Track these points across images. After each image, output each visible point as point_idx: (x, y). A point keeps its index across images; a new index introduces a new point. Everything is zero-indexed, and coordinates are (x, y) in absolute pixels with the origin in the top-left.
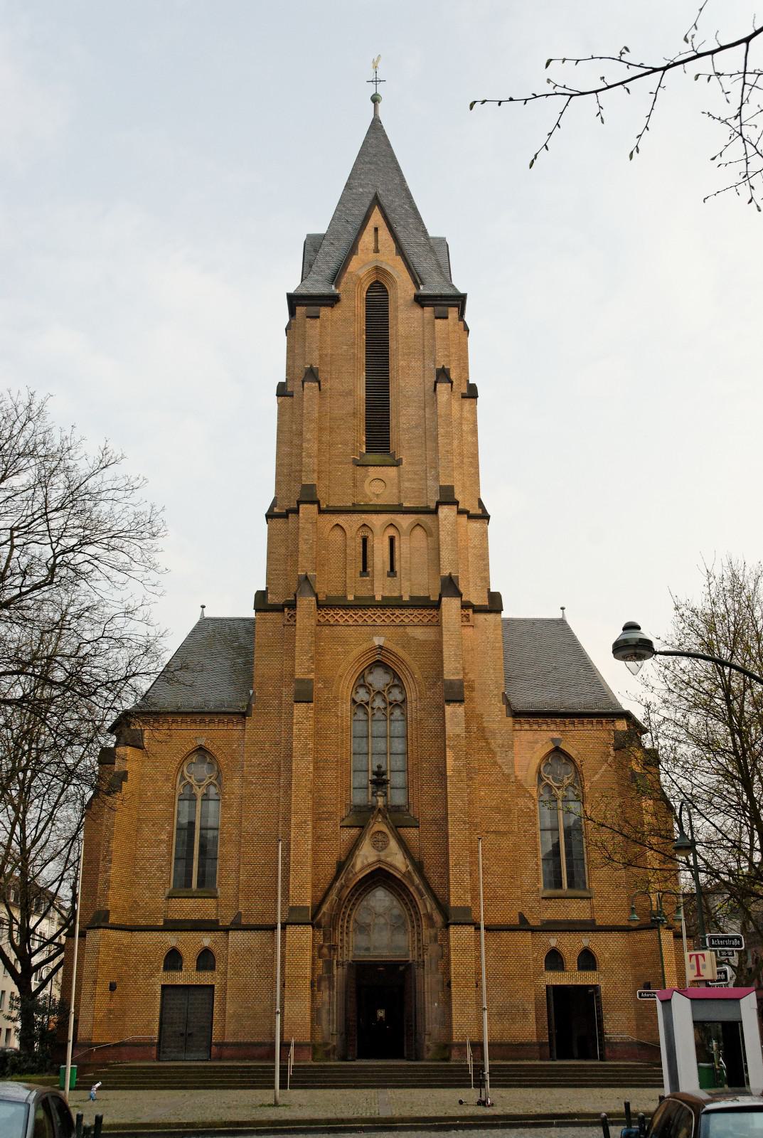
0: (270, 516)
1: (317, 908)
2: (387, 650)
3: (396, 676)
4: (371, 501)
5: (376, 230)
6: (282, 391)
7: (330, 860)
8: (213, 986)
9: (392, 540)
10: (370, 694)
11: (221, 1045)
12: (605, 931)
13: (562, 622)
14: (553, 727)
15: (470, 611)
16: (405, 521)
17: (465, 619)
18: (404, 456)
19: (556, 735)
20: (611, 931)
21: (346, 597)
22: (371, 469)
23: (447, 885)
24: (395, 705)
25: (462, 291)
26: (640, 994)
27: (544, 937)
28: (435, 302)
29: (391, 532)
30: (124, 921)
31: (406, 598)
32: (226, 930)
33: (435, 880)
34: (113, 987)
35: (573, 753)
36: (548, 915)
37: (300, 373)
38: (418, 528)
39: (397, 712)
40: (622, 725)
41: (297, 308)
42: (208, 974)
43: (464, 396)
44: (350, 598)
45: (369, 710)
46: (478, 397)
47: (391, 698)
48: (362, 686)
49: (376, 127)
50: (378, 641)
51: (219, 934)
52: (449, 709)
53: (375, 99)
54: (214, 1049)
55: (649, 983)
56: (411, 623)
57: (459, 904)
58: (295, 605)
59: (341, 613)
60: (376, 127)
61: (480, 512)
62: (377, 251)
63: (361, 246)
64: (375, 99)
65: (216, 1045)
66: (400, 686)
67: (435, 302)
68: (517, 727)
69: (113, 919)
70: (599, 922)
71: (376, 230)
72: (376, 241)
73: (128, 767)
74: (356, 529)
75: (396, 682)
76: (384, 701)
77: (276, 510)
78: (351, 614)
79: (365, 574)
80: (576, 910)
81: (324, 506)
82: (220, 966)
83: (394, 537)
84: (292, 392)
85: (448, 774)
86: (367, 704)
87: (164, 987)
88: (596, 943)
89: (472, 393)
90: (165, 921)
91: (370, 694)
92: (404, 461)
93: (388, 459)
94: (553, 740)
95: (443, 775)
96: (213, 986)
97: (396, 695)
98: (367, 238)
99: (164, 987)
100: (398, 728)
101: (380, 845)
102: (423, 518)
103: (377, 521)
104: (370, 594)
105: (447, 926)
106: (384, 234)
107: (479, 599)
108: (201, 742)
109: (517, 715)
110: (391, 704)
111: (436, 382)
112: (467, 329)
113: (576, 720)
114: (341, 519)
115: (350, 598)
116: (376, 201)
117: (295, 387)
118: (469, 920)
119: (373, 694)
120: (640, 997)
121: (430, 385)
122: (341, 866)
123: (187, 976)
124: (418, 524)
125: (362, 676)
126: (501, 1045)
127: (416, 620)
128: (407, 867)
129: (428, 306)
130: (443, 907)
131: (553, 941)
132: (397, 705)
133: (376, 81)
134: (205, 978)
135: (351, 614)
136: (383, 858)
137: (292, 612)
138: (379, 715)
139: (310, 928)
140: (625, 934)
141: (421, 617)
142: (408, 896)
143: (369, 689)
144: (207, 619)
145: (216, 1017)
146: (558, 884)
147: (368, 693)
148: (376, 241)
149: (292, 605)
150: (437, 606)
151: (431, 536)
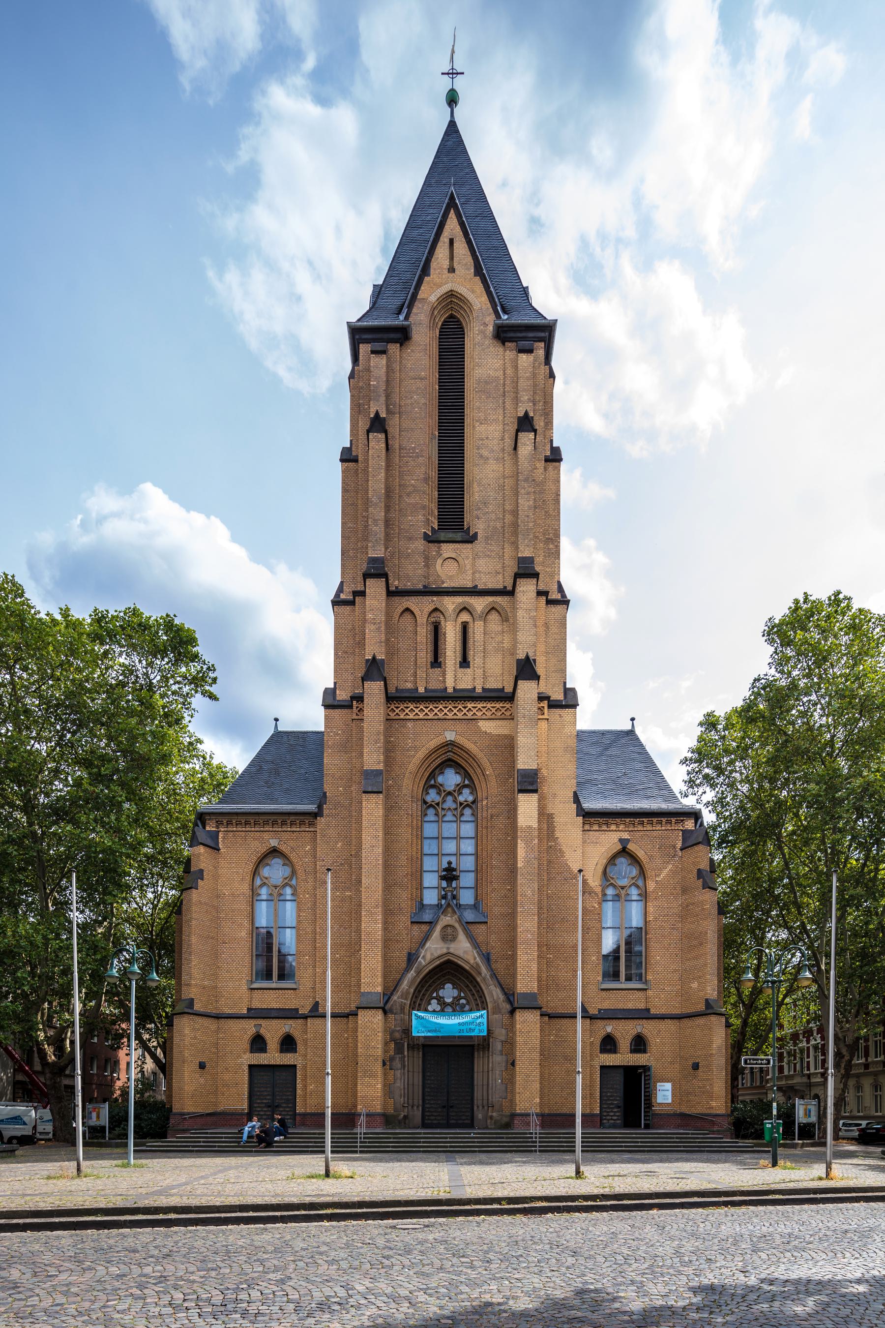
0: (337, 602)
1: (388, 994)
2: (461, 747)
3: (467, 775)
4: (443, 583)
5: (451, 242)
6: (348, 457)
7: (400, 957)
8: (295, 1066)
9: (465, 627)
10: (440, 796)
11: (304, 1115)
12: (658, 1018)
13: (631, 733)
14: (622, 827)
15: (545, 704)
16: (479, 604)
17: (540, 712)
18: (479, 527)
19: (626, 836)
20: (663, 1018)
21: (417, 689)
22: (444, 546)
23: (514, 976)
24: (465, 805)
25: (549, 317)
26: (746, 1061)
27: (600, 1023)
28: (519, 335)
29: (465, 617)
30: (210, 1009)
31: (479, 690)
32: (305, 1017)
33: (500, 967)
34: (202, 1066)
35: (641, 854)
36: (606, 1005)
37: (364, 425)
38: (493, 612)
39: (468, 812)
40: (690, 824)
41: (361, 345)
42: (289, 1055)
43: (547, 460)
44: (421, 690)
45: (440, 810)
46: (561, 460)
47: (461, 799)
48: (433, 786)
49: (452, 129)
50: (450, 736)
51: (300, 1021)
52: (522, 797)
53: (452, 99)
54: (298, 1118)
55: (698, 1063)
56: (484, 717)
57: (524, 990)
58: (363, 697)
59: (412, 707)
60: (452, 129)
61: (559, 597)
62: (452, 270)
63: (433, 264)
64: (452, 99)
65: (300, 1114)
66: (472, 788)
67: (519, 335)
68: (587, 827)
69: (197, 1007)
70: (653, 1011)
71: (451, 242)
72: (452, 258)
73: (202, 866)
74: (427, 614)
75: (467, 782)
76: (455, 801)
77: (343, 596)
78: (421, 707)
79: (436, 665)
80: (634, 1002)
81: (395, 583)
82: (300, 1047)
83: (467, 623)
84: (357, 456)
85: (519, 865)
86: (438, 804)
87: (250, 1066)
88: (646, 1028)
89: (555, 457)
90: (249, 1010)
91: (440, 796)
92: (479, 536)
93: (459, 536)
94: (621, 840)
95: (513, 870)
96: (295, 1066)
97: (466, 796)
98: (442, 252)
99: (250, 1066)
100: (468, 829)
101: (448, 936)
102: (499, 599)
103: (450, 604)
104: (441, 686)
105: (512, 1012)
106: (461, 247)
107: (557, 695)
108: (274, 843)
109: (587, 815)
110: (461, 804)
111: (517, 431)
112: (552, 375)
113: (645, 820)
114: (411, 603)
115: (421, 690)
116: (452, 204)
117: (359, 452)
118: (534, 1004)
119: (443, 794)
120: (769, 1061)
121: (509, 442)
122: (411, 958)
123: (273, 1056)
124: (493, 608)
125: (432, 775)
126: (117, 1146)
127: (489, 714)
128: (475, 958)
129: (511, 340)
130: (509, 995)
131: (609, 1028)
132: (468, 805)
133: (453, 74)
134: (287, 1059)
135: (421, 707)
136: (452, 951)
137: (361, 706)
138: (449, 817)
139: (380, 1013)
140: (676, 1021)
141: (494, 710)
142: (475, 986)
143: (440, 790)
144: (280, 732)
145: (299, 1092)
146: (616, 976)
147: (439, 793)
148: (452, 258)
149: (360, 698)
150: (511, 698)
151: (507, 620)
